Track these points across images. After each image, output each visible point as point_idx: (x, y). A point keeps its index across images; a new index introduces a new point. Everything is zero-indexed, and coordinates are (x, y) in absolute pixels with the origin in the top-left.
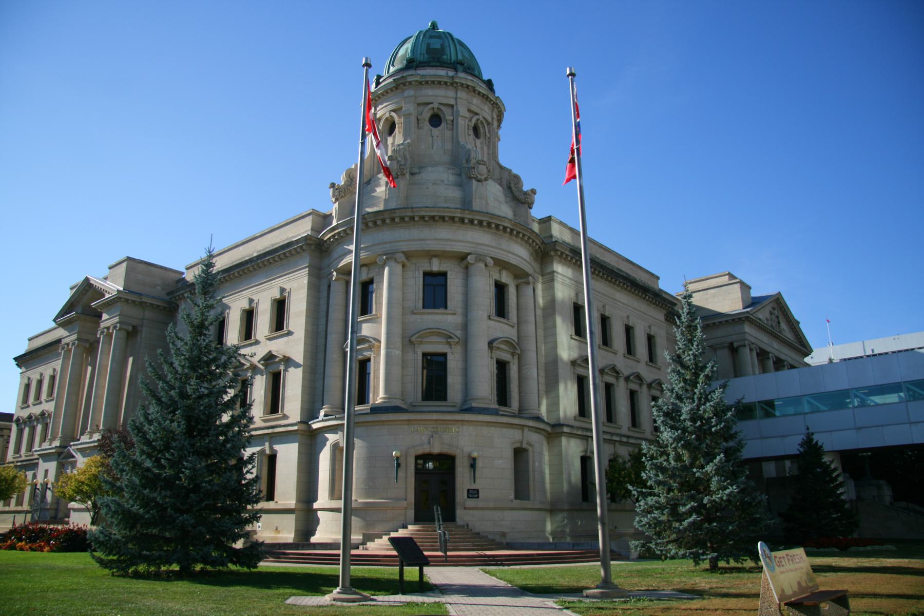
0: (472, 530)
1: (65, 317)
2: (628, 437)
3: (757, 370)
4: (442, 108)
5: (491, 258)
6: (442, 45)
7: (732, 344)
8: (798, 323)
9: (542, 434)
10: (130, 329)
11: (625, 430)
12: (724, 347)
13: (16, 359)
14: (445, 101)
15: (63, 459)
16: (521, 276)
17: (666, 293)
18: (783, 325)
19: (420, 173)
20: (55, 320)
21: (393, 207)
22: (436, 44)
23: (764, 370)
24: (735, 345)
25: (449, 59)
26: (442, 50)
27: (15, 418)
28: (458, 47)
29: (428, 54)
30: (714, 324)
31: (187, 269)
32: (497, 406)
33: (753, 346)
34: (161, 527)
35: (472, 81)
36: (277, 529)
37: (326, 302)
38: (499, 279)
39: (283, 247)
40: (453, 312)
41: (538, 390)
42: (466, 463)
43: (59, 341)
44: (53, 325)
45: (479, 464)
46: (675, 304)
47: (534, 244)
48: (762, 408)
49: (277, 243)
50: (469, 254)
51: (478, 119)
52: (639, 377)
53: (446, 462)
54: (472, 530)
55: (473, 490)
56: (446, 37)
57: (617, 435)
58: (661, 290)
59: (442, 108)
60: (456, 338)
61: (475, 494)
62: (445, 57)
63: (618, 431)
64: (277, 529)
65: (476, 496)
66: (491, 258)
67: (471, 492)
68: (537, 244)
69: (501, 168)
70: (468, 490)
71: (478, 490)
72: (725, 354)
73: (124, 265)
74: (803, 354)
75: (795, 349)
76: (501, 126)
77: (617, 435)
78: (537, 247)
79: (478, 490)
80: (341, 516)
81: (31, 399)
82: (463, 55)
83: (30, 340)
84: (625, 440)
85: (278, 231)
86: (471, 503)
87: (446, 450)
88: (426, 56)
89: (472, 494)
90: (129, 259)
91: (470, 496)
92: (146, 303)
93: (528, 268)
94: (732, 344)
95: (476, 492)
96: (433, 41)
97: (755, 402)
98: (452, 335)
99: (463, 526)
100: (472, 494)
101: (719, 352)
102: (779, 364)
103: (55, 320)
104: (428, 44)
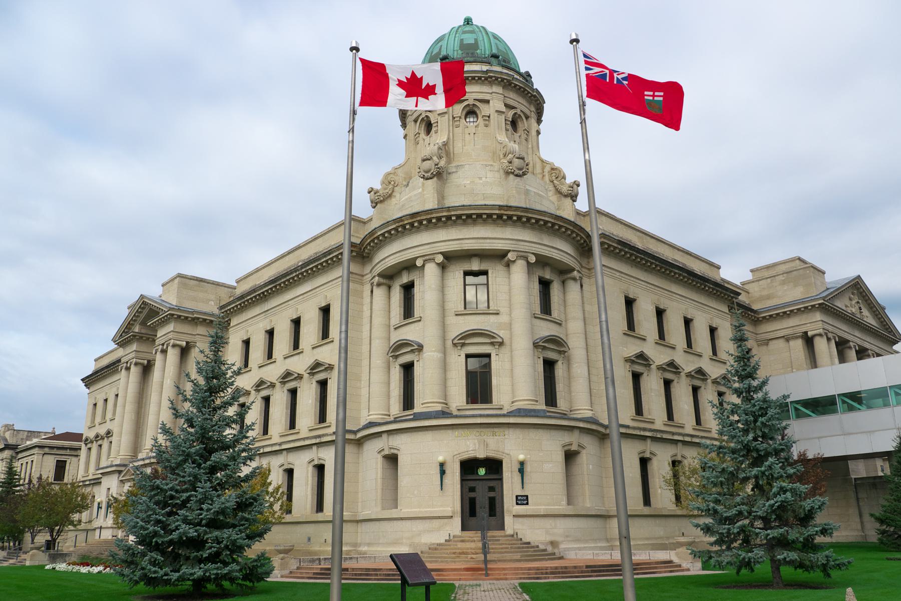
0: (521, 539)
1: (124, 338)
2: (692, 436)
3: (837, 360)
4: (478, 104)
5: (533, 253)
6: (476, 40)
7: (806, 333)
8: (883, 309)
9: (595, 435)
10: (184, 344)
11: (689, 429)
12: (797, 338)
13: (83, 380)
14: (480, 97)
15: (123, 477)
16: (564, 271)
17: (728, 283)
18: (866, 312)
19: (457, 172)
20: (114, 340)
21: (431, 208)
22: (469, 39)
23: (842, 359)
24: (810, 334)
25: (483, 53)
26: (475, 45)
27: (84, 438)
28: (492, 38)
29: (462, 51)
30: (785, 313)
31: (238, 282)
32: (544, 407)
33: (830, 335)
34: (169, 527)
35: (508, 74)
36: (325, 542)
37: (369, 308)
38: (542, 275)
39: (325, 254)
40: (495, 312)
41: (590, 389)
42: (516, 467)
43: (119, 361)
44: (113, 346)
45: (528, 468)
46: (739, 294)
47: (579, 238)
48: (844, 402)
49: (320, 252)
50: (509, 251)
51: (515, 113)
52: (700, 372)
53: (494, 466)
54: (521, 539)
55: (522, 496)
56: (480, 31)
57: (679, 434)
58: (722, 280)
59: (478, 104)
60: (499, 338)
61: (524, 500)
62: (478, 51)
63: (680, 431)
64: (325, 542)
65: (525, 502)
66: (533, 253)
67: (519, 498)
68: (582, 238)
69: (542, 161)
70: (517, 497)
71: (527, 496)
72: (798, 345)
73: (177, 281)
74: (891, 342)
75: (881, 337)
76: (543, 119)
77: (679, 434)
78: (582, 241)
79: (527, 496)
80: (347, 515)
81: (98, 419)
82: (498, 49)
83: (96, 360)
84: (688, 439)
85: (321, 238)
86: (521, 509)
87: (492, 454)
88: (460, 52)
89: (520, 500)
90: (180, 276)
91: (519, 502)
92: (198, 318)
93: (571, 262)
94: (806, 333)
95: (525, 498)
96: (465, 36)
97: (835, 395)
98: (494, 335)
99: (513, 536)
100: (520, 500)
101: (792, 343)
102: (862, 354)
103: (114, 340)
104: (462, 40)
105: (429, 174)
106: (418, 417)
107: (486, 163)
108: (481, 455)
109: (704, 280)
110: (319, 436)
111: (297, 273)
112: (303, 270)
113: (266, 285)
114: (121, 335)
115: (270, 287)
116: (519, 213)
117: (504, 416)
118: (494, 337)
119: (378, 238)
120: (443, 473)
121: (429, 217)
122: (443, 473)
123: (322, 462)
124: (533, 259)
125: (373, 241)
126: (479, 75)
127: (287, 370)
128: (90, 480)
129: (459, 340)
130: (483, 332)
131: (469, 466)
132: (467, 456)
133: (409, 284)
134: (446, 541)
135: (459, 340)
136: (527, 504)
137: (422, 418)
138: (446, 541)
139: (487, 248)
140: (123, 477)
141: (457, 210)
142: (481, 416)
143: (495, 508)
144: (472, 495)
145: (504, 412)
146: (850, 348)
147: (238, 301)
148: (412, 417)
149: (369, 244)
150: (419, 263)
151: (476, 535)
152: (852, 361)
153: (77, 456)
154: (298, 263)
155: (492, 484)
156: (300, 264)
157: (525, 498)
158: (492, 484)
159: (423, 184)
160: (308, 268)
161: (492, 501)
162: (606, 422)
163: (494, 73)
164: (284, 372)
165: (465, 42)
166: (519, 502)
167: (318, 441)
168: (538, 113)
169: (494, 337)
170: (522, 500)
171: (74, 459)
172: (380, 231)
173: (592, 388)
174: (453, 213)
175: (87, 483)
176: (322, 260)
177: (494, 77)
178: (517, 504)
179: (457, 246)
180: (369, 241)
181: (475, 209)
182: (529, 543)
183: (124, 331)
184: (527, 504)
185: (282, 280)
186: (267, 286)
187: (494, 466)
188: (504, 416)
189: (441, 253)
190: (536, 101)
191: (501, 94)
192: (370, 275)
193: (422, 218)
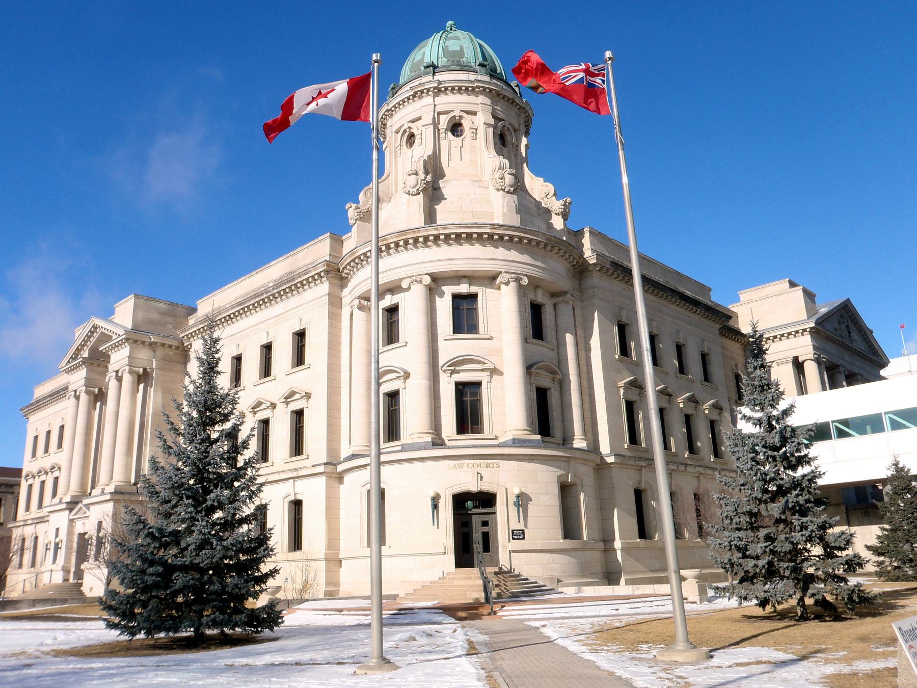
5: (525, 275)
6: (462, 47)
14: (467, 108)
15: (75, 515)
24: (801, 360)
55: (518, 530)
59: (464, 114)
62: (464, 59)
66: (525, 275)
67: (515, 532)
91: (515, 537)
95: (521, 532)
105: (415, 190)
106: (404, 448)
107: (474, 179)
108: (474, 488)
109: (695, 303)
110: (296, 470)
111: (269, 294)
112: (275, 291)
113: (232, 307)
114: (69, 362)
115: (237, 309)
116: (501, 232)
117: (499, 446)
118: (484, 363)
119: (359, 257)
120: (435, 507)
121: (415, 235)
122: (435, 507)
123: (299, 497)
124: (525, 282)
125: (353, 260)
126: (467, 85)
127: (258, 398)
128: (33, 519)
129: (447, 367)
130: (476, 358)
131: (460, 500)
132: (460, 489)
133: (393, 307)
134: (439, 579)
135: (447, 367)
136: (524, 538)
137: (412, 449)
138: (439, 579)
139: (477, 269)
140: (75, 515)
141: (445, 229)
142: (474, 447)
143: (487, 543)
144: (486, 529)
145: (502, 440)
146: (840, 372)
147: (201, 323)
148: (399, 448)
149: (349, 264)
150: (405, 285)
151: (474, 572)
152: (20, 481)
153: (13, 493)
154: (269, 283)
155: (486, 518)
156: (271, 284)
157: (521, 532)
158: (486, 518)
159: (409, 201)
160: (280, 289)
161: (486, 536)
162: (92, 495)
163: (482, 83)
164: (255, 400)
165: (450, 49)
166: (515, 537)
167: (295, 474)
168: (526, 126)
169: (484, 363)
170: (518, 535)
171: (10, 497)
172: (361, 249)
173: (585, 416)
174: (441, 232)
175: (30, 522)
176: (297, 281)
177: (482, 87)
178: (513, 539)
179: (445, 267)
180: (349, 261)
181: (465, 228)
182: (527, 579)
183: (71, 357)
184: (524, 538)
185: (252, 302)
186: (234, 308)
187: (487, 500)
188: (499, 446)
189: (427, 274)
190: (525, 113)
191: (489, 105)
192: (350, 296)
193: (408, 236)
